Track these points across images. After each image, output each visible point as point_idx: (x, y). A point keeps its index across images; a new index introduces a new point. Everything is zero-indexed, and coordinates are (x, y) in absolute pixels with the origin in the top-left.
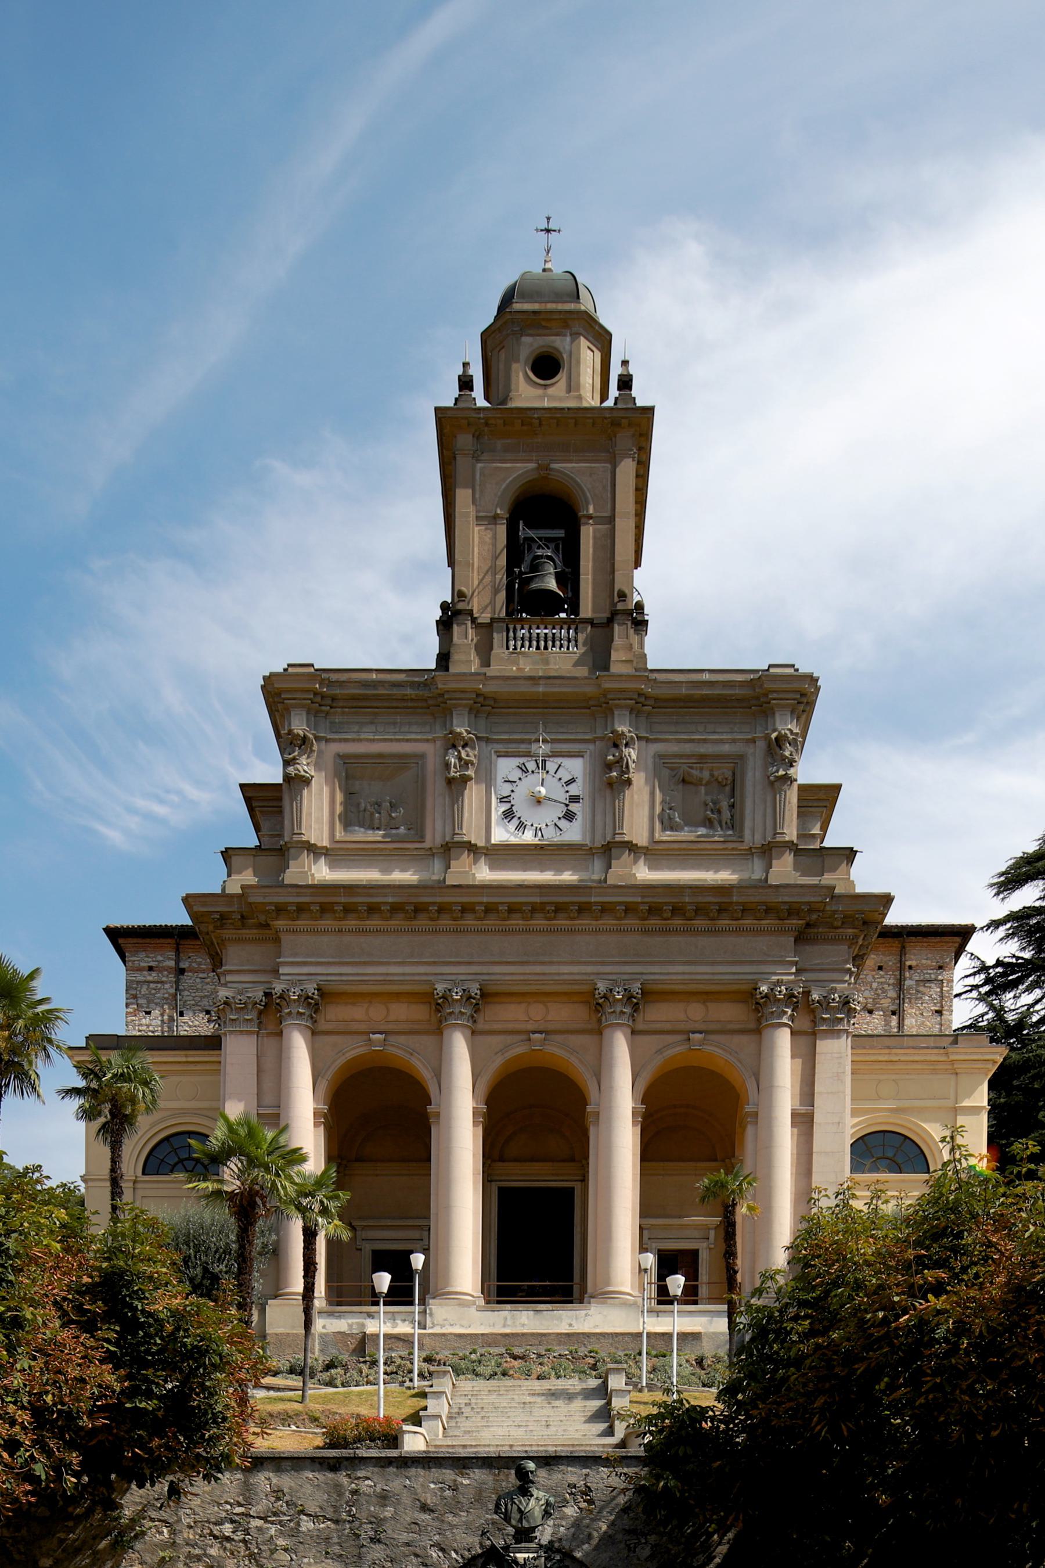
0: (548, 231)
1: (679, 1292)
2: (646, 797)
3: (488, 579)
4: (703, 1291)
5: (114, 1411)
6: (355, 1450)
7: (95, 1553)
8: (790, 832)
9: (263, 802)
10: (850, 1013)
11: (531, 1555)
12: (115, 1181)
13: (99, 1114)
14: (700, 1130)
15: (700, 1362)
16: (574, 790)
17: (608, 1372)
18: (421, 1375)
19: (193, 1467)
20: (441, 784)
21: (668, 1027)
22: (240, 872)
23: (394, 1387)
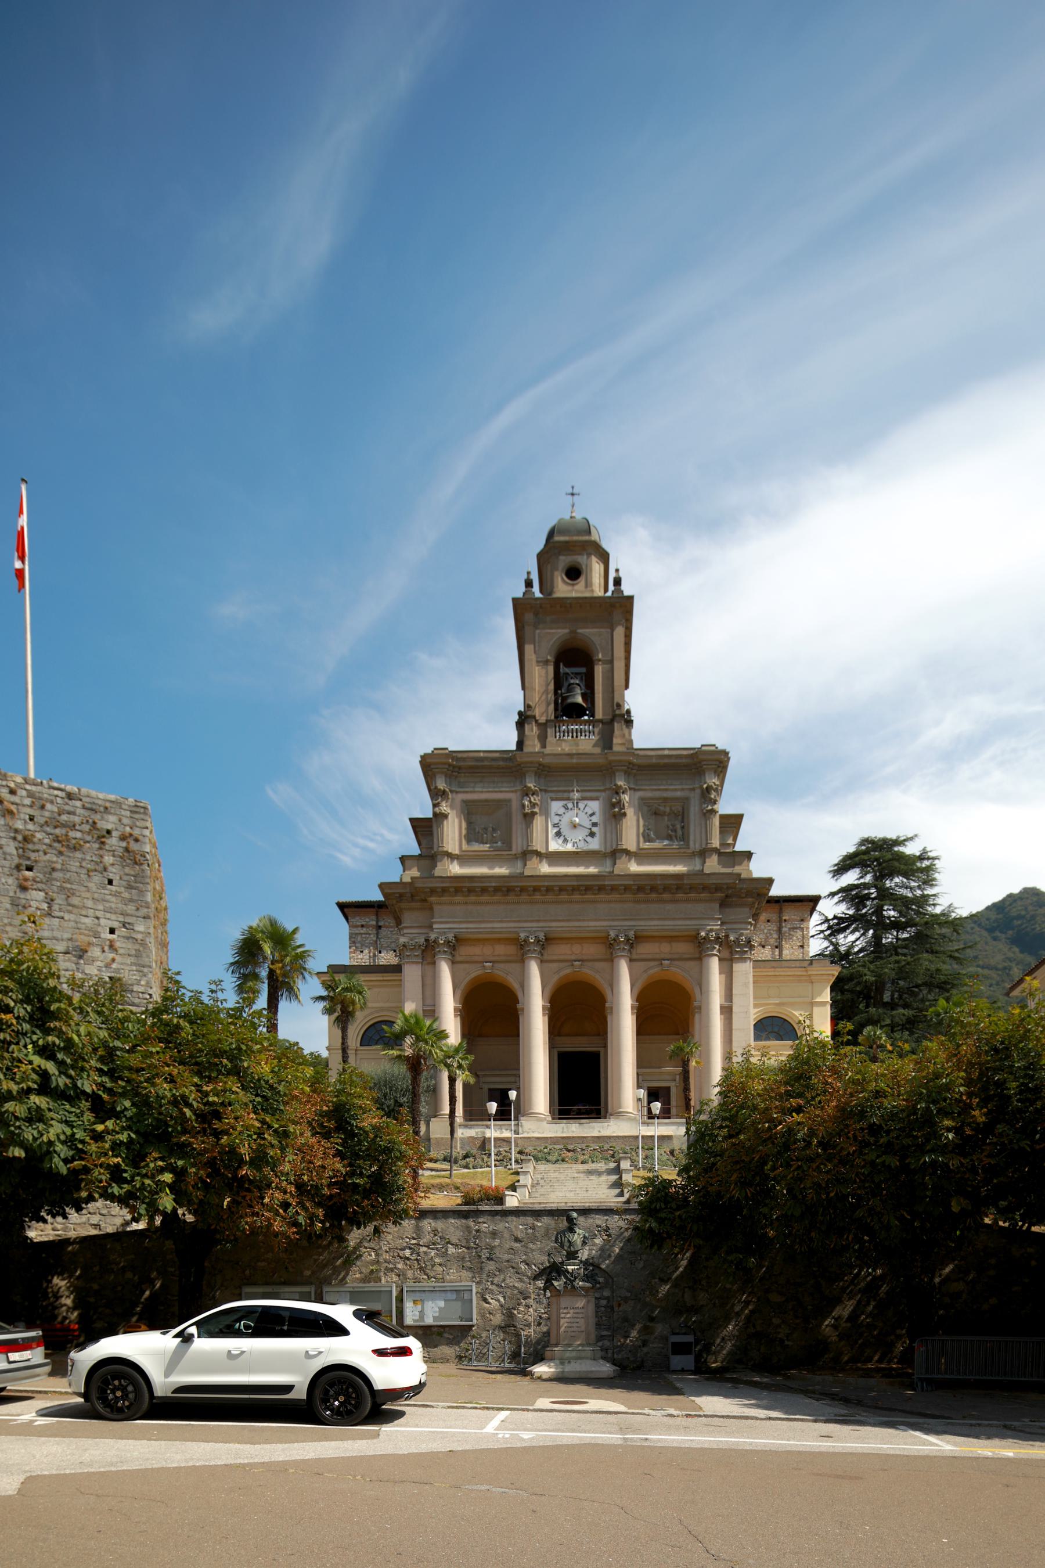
0: (573, 494)
1: (658, 1112)
2: (635, 823)
3: (544, 697)
4: (673, 1111)
5: (342, 1185)
6: (482, 1205)
7: (335, 1268)
8: (716, 843)
9: (424, 828)
10: (752, 947)
12: (344, 1050)
13: (335, 1011)
14: (669, 1016)
15: (672, 1152)
16: (595, 819)
17: (620, 1159)
18: (516, 1161)
19: (387, 1217)
20: (520, 817)
21: (650, 957)
22: (410, 869)
23: (501, 1168)
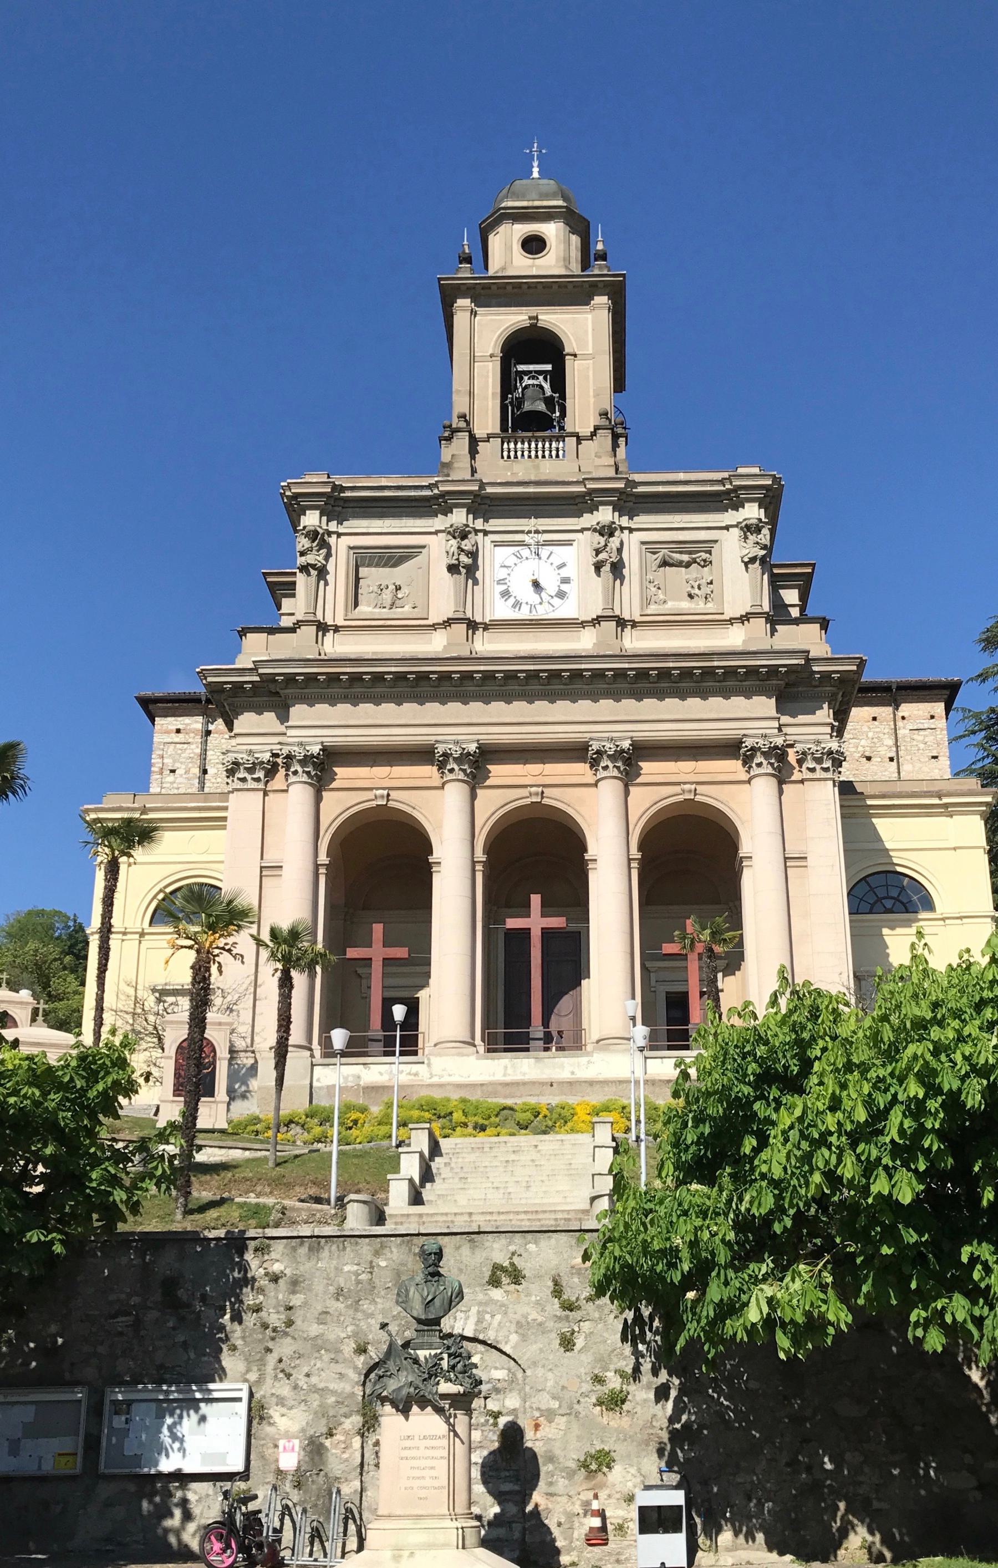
11: (433, 1352)
16: (564, 573)
